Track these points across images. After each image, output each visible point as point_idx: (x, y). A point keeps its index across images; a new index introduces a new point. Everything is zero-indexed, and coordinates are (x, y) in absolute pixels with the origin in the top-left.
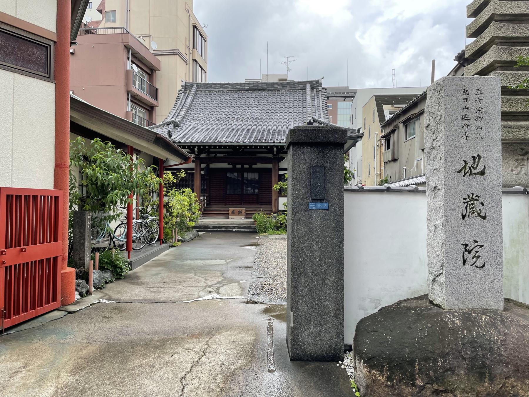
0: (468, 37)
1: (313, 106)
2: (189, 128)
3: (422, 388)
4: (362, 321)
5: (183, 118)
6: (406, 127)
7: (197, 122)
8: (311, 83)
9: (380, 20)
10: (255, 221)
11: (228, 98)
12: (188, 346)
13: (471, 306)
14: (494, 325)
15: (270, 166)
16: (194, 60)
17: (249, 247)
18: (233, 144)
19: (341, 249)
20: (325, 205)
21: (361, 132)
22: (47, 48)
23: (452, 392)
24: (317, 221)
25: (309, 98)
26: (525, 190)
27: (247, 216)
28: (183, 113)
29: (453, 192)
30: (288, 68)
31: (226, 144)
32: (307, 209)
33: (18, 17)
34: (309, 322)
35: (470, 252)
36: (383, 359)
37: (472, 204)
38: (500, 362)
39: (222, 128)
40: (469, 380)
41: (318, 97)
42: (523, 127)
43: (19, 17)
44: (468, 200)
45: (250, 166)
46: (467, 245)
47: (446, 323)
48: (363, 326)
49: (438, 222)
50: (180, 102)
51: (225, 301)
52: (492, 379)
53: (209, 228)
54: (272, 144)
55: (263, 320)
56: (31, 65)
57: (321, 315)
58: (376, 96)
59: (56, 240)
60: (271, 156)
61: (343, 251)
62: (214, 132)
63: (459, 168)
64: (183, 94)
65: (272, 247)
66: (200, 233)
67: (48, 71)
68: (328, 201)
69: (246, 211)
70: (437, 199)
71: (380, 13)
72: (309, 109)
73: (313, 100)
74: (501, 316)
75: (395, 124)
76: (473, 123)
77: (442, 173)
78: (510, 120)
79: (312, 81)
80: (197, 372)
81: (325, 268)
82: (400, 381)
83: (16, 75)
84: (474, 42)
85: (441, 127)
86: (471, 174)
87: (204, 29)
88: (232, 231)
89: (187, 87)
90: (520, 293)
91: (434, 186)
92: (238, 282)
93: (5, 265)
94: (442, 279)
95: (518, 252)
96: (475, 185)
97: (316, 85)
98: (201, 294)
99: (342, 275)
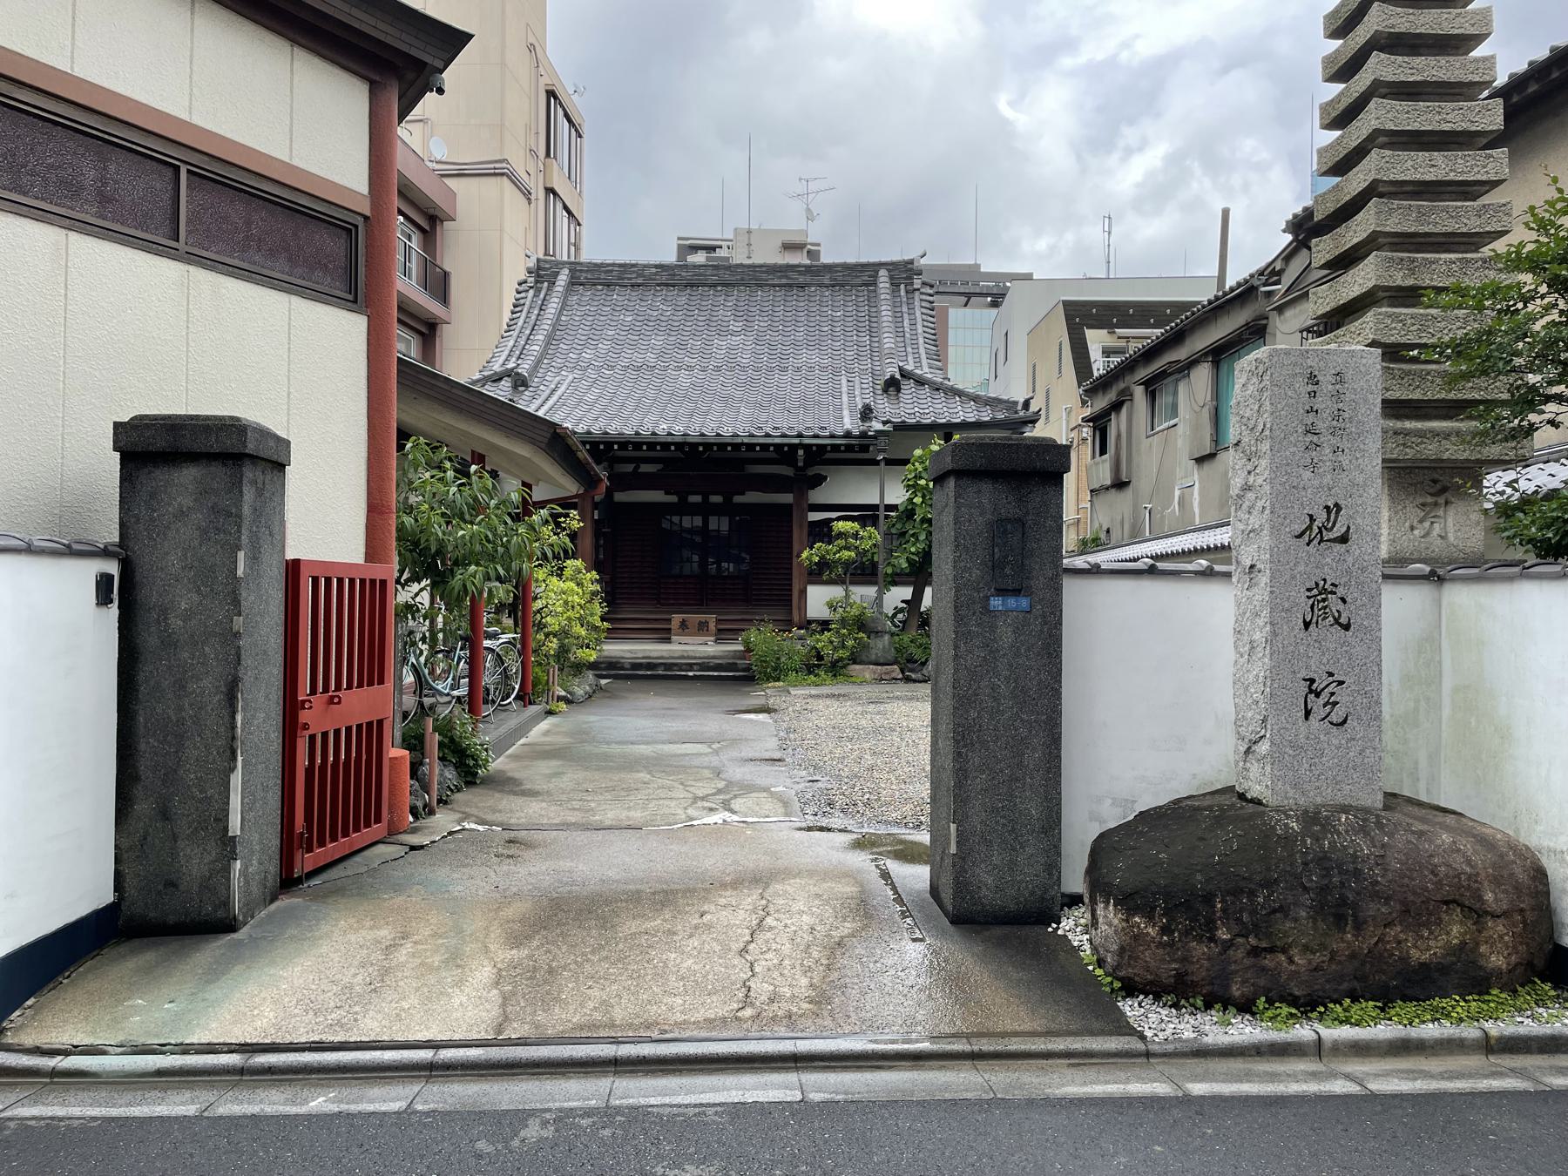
0: (1326, 81)
1: (899, 333)
2: (559, 393)
3: (1227, 945)
4: (1102, 836)
5: (538, 362)
6: (1152, 396)
7: (577, 374)
8: (892, 267)
9: (1067, 62)
10: (748, 650)
11: (661, 305)
12: (722, 901)
13: (1319, 800)
14: (1364, 830)
15: (787, 498)
16: (550, 191)
17: (752, 716)
18: (690, 440)
19: (1057, 694)
20: (1024, 603)
21: (1033, 408)
22: (349, 231)
23: (1284, 951)
24: (1005, 635)
25: (886, 312)
26: (1433, 573)
27: (722, 635)
28: (536, 348)
29: (1287, 577)
30: (808, 210)
31: (669, 439)
32: (986, 610)
33: (296, 162)
34: (989, 843)
35: (1318, 695)
36: (1154, 894)
37: (1324, 600)
38: (1376, 895)
39: (651, 393)
40: (1315, 928)
41: (911, 309)
42: (1436, 434)
43: (79, 72)
44: (1315, 592)
45: (728, 499)
46: (1312, 681)
47: (1273, 828)
48: (1103, 847)
49: (1257, 636)
50: (524, 314)
51: (758, 826)
52: (1359, 927)
53: (623, 668)
54: (796, 441)
55: (861, 861)
56: (318, 274)
57: (1013, 829)
58: (1066, 304)
59: (381, 682)
60: (787, 471)
61: (1059, 698)
62: (631, 405)
63: (1299, 528)
64: (531, 292)
65: (813, 716)
66: (603, 682)
67: (353, 287)
68: (1029, 594)
69: (719, 621)
70: (1255, 590)
71: (1069, 44)
72: (888, 341)
73: (898, 318)
74: (1377, 816)
75: (1122, 385)
76: (1327, 440)
77: (1266, 539)
78: (1408, 417)
79: (892, 264)
80: (767, 942)
81: (1023, 732)
82: (1187, 932)
83: (294, 299)
84: (1338, 141)
85: (1265, 447)
86: (1321, 541)
87: (575, 97)
88: (686, 677)
89: (542, 274)
90: (1422, 786)
91: (1249, 563)
92: (766, 790)
93: (311, 732)
94: (1263, 748)
95: (1417, 701)
96: (1328, 563)
97: (904, 273)
98: (691, 812)
99: (1059, 749)
